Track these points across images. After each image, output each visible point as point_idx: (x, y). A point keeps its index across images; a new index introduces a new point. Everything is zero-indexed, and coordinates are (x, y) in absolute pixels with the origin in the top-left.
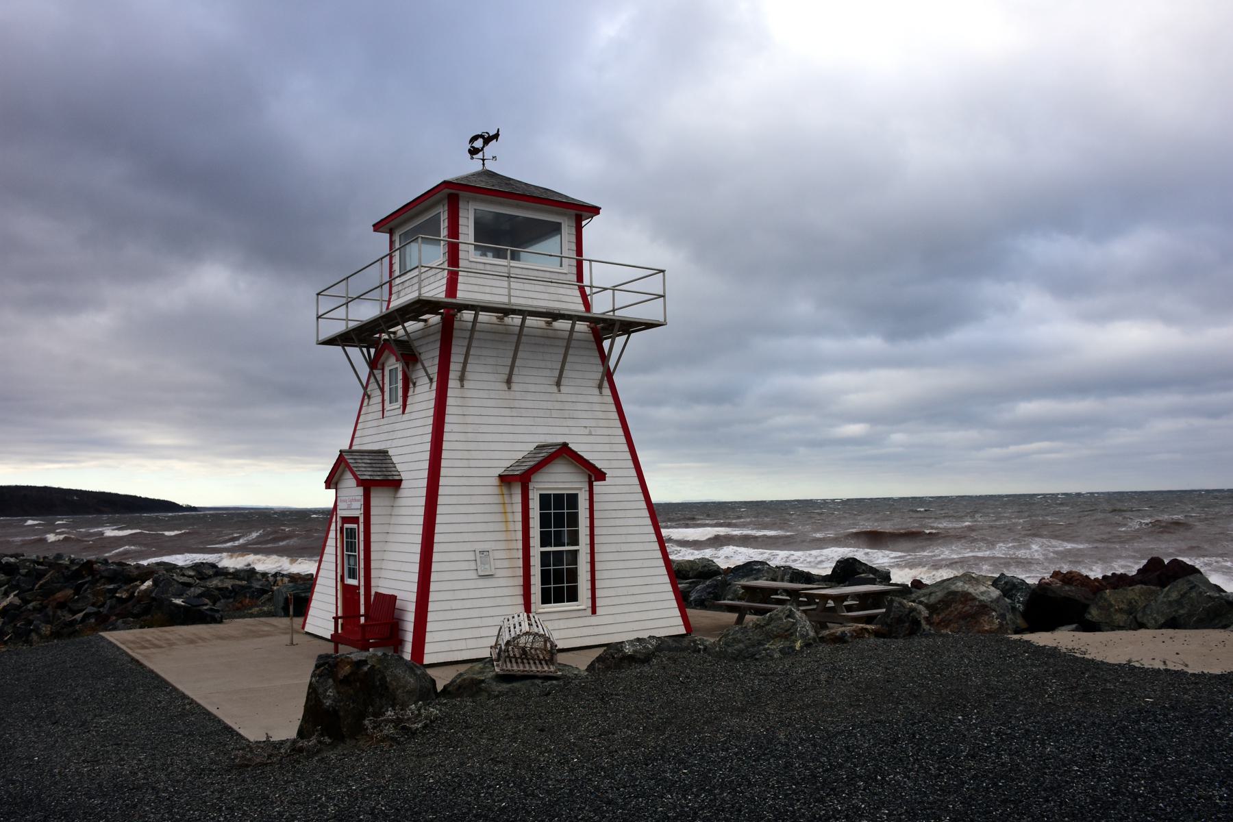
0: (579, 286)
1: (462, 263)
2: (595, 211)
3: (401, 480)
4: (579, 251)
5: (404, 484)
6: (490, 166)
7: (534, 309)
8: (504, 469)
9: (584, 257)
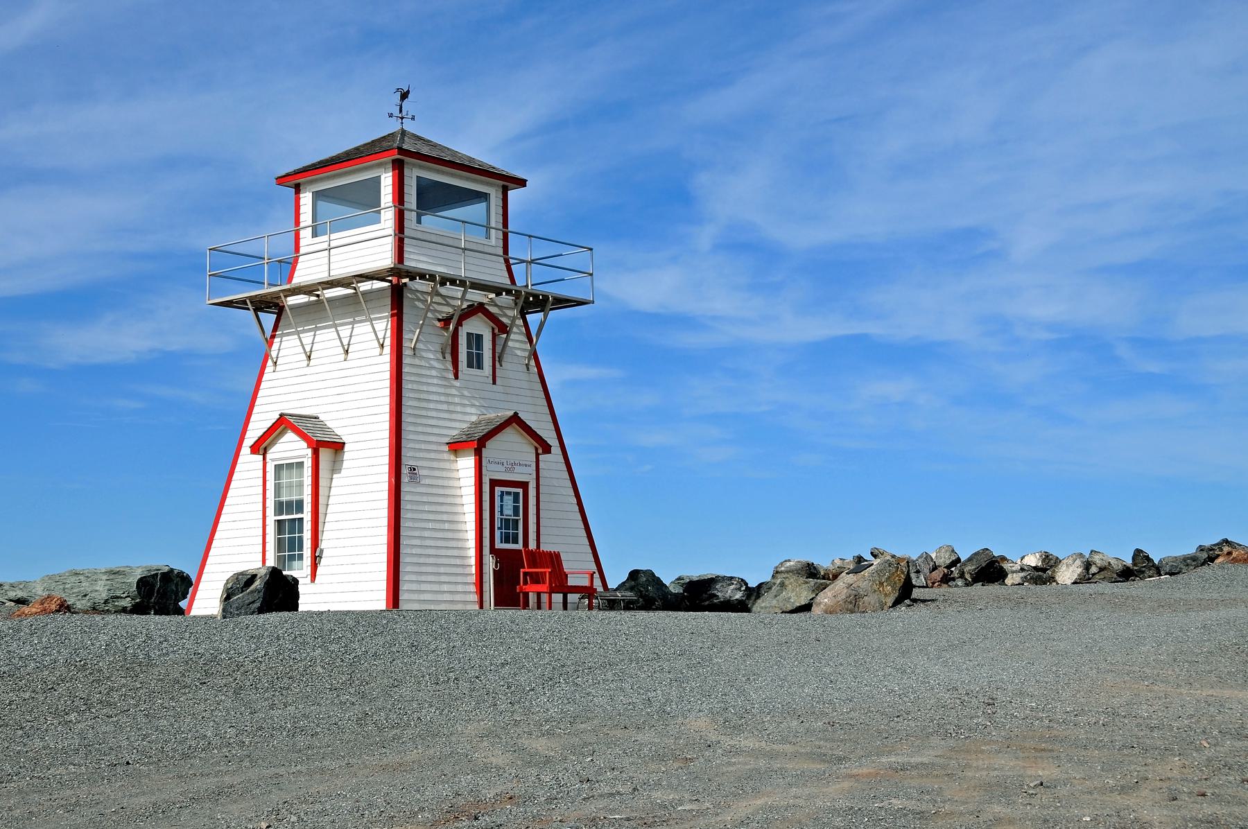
0: (505, 259)
1: (406, 230)
2: (522, 183)
3: (344, 443)
4: (505, 224)
5: (347, 448)
6: (409, 126)
7: (477, 281)
8: (468, 425)
9: (510, 229)
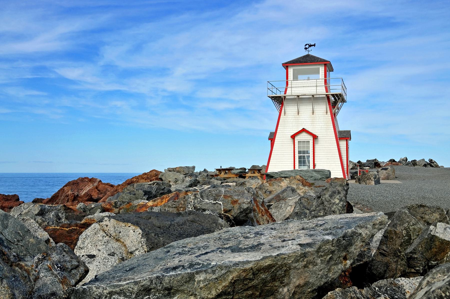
5: (319, 138)
